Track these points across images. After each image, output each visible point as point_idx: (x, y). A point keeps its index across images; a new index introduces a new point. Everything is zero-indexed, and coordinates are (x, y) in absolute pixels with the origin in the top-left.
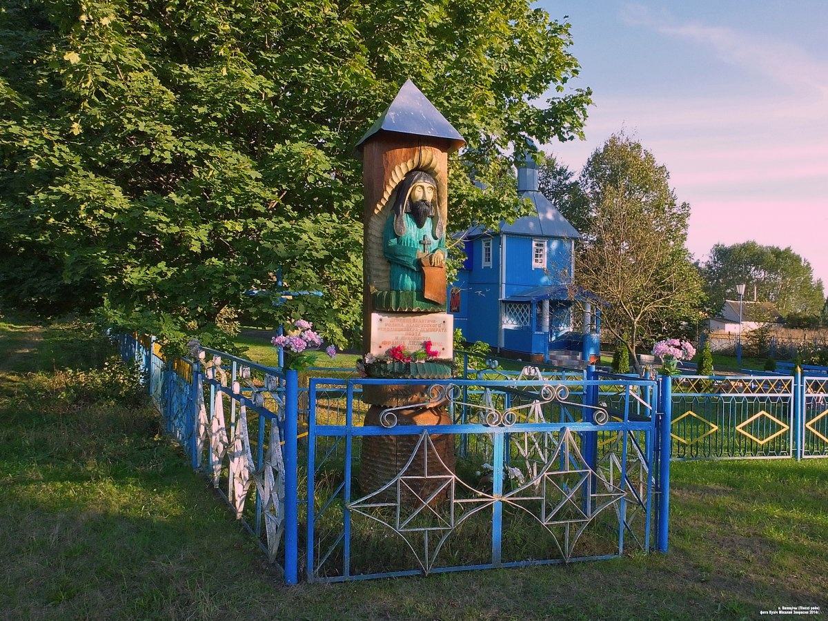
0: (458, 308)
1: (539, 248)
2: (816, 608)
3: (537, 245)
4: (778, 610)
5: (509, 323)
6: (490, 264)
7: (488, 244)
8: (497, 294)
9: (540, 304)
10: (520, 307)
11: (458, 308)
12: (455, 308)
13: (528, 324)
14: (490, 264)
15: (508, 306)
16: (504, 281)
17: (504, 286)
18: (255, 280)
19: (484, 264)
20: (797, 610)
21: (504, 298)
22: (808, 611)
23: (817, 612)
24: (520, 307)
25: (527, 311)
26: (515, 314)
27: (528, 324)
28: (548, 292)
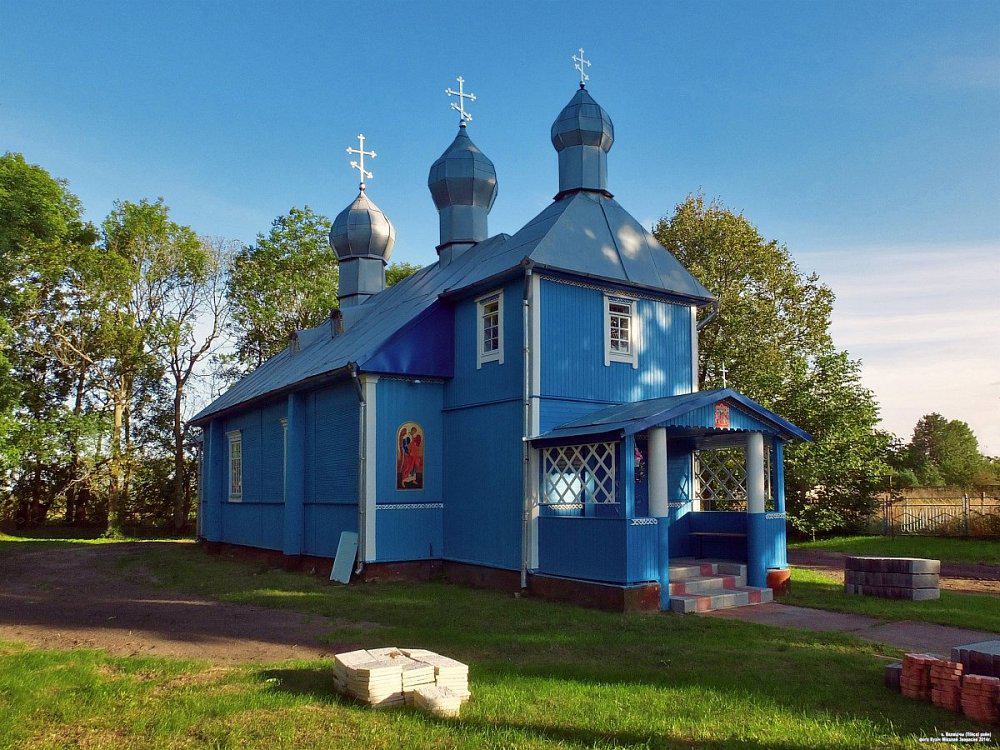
0: (419, 479)
1: (619, 315)
2: (986, 734)
3: (613, 308)
4: (941, 737)
5: (566, 491)
6: (499, 355)
7: (495, 307)
8: (519, 423)
9: (643, 443)
10: (569, 454)
11: (419, 479)
12: (411, 478)
13: (611, 498)
14: (499, 355)
15: (547, 455)
16: (537, 391)
17: (536, 402)
18: (173, 473)
19: (483, 356)
20: (964, 737)
21: (536, 434)
22: (978, 738)
23: (988, 740)
24: (569, 454)
25: (608, 462)
26: (593, 462)
27: (611, 498)
28: (659, 414)
